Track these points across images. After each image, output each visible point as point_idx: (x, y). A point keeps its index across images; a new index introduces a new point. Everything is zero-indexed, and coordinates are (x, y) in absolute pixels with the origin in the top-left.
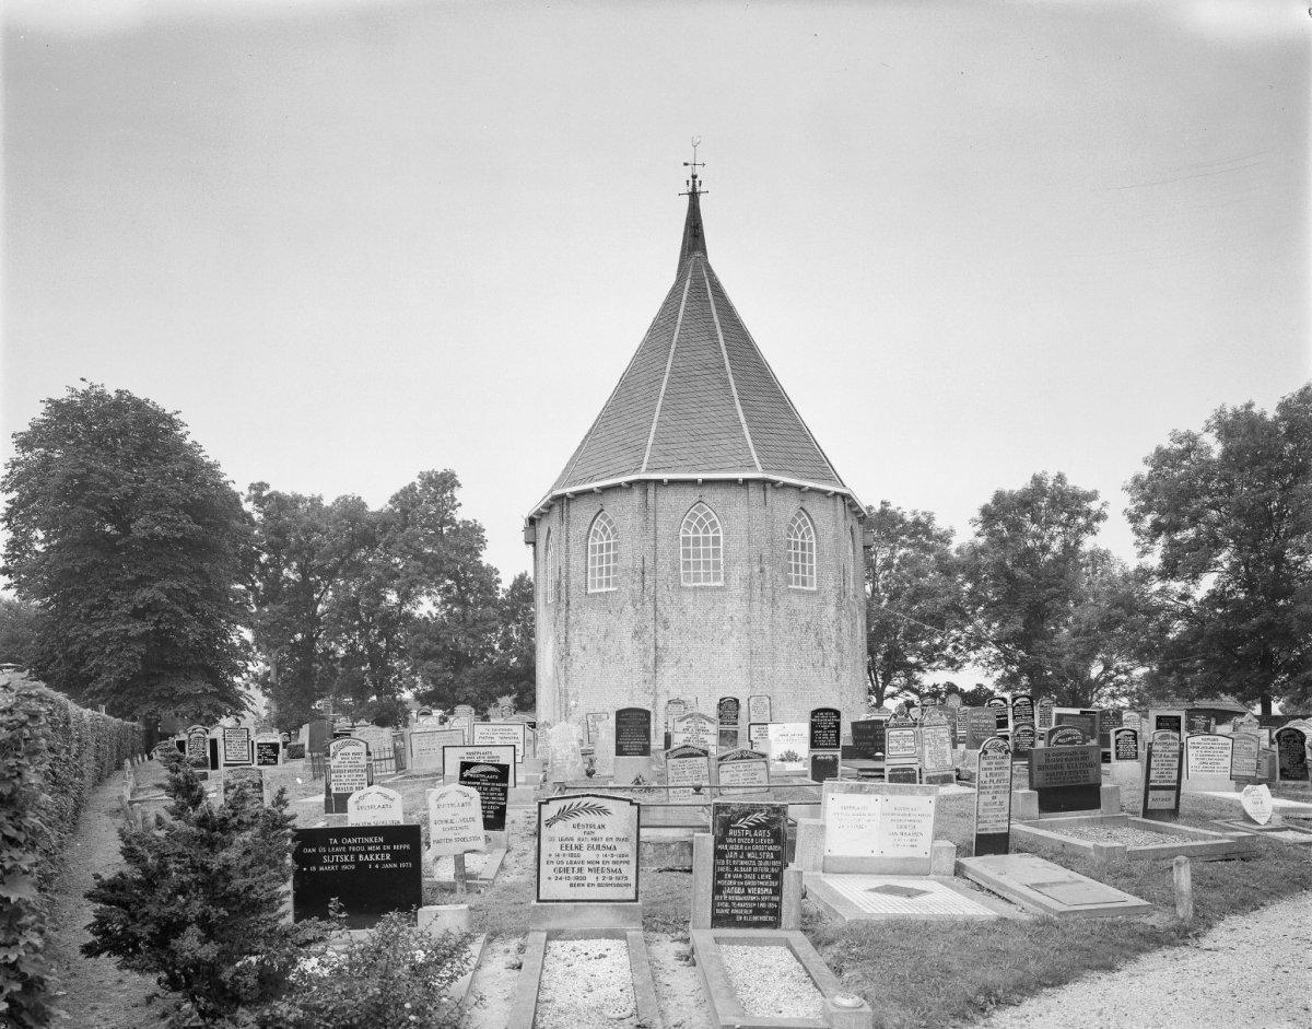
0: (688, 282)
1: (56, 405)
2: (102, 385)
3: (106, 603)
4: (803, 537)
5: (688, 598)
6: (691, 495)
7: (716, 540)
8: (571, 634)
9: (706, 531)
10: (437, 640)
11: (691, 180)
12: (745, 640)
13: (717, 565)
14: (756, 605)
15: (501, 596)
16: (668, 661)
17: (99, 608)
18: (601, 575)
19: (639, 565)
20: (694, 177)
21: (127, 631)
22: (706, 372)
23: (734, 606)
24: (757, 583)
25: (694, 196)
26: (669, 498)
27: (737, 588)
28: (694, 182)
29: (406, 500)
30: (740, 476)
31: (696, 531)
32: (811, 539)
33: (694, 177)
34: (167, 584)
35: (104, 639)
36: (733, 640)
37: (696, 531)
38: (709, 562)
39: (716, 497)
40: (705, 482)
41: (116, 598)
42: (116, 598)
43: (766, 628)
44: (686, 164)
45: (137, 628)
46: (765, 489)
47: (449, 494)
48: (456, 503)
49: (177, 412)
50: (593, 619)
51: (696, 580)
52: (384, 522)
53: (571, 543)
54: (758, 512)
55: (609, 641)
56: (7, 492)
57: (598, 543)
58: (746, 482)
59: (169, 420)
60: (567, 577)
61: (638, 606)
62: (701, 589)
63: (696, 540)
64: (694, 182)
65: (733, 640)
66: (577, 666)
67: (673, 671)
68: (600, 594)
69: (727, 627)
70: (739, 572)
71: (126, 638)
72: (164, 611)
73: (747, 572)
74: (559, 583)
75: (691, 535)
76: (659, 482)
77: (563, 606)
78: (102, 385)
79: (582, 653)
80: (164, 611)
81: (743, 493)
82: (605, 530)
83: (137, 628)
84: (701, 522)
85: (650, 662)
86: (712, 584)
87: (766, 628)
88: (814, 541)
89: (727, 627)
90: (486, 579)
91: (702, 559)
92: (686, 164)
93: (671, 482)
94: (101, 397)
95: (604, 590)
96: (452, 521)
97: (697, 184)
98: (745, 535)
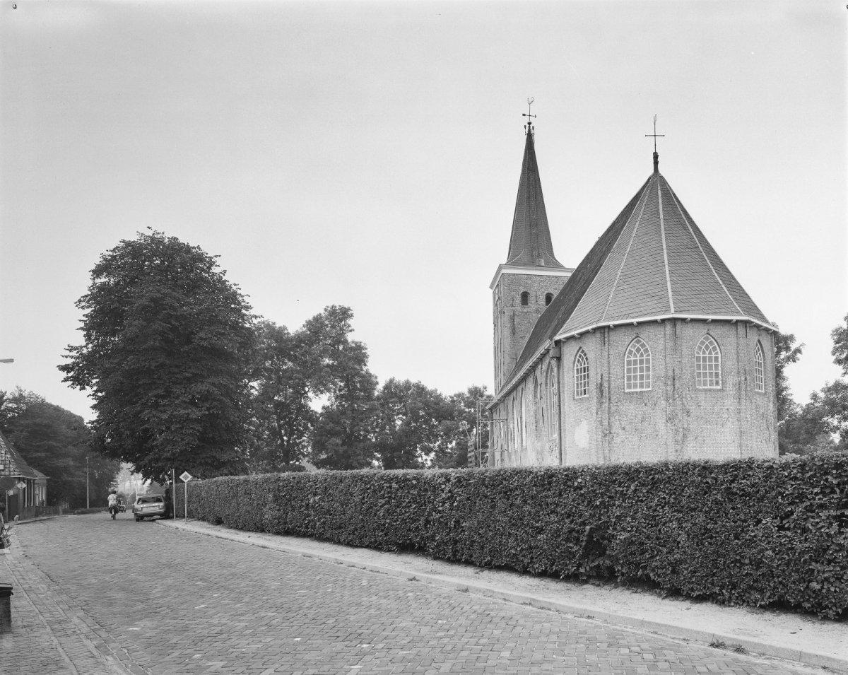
0: (660, 193)
1: (128, 244)
2: (163, 233)
3: (168, 394)
4: (642, 355)
5: (702, 396)
6: (702, 330)
7: (716, 359)
8: (612, 419)
9: (710, 353)
10: (338, 423)
11: (527, 126)
12: (736, 423)
13: (717, 375)
14: (743, 402)
15: (376, 393)
16: (690, 438)
17: (163, 397)
18: (636, 380)
19: (670, 374)
20: (529, 124)
21: (188, 414)
22: (687, 250)
23: (730, 403)
24: (743, 387)
25: (530, 137)
26: (687, 332)
27: (731, 390)
28: (529, 127)
29: (316, 326)
30: (659, 317)
31: (704, 353)
32: (717, 353)
33: (529, 124)
34: (216, 380)
35: (170, 420)
36: (729, 424)
37: (704, 353)
38: (630, 376)
39: (717, 331)
40: (714, 321)
41: (177, 390)
42: (177, 390)
43: (748, 416)
44: (524, 115)
45: (195, 413)
46: (746, 327)
47: (343, 322)
48: (350, 328)
49: (216, 256)
50: (631, 410)
51: (704, 385)
52: (300, 340)
53: (611, 357)
54: (742, 341)
55: (646, 424)
56: (83, 308)
57: (632, 359)
58: (663, 321)
59: (200, 258)
60: (609, 381)
61: (671, 401)
62: (710, 390)
63: (635, 362)
64: (529, 127)
65: (729, 424)
66: (617, 440)
67: (693, 444)
68: (636, 392)
69: (725, 416)
70: (732, 380)
71: (188, 419)
72: (214, 400)
73: (737, 379)
74: (601, 385)
75: (701, 355)
76: (684, 320)
77: (605, 400)
78: (163, 233)
79: (621, 432)
80: (214, 400)
81: (661, 329)
82: (638, 350)
83: (195, 413)
84: (707, 347)
85: (680, 437)
86: (715, 387)
87: (748, 416)
88: (719, 355)
89: (725, 416)
90: (368, 381)
91: (708, 371)
92: (524, 115)
93: (693, 320)
94: (160, 242)
95: (638, 390)
96: (346, 341)
97: (531, 128)
98: (735, 357)
